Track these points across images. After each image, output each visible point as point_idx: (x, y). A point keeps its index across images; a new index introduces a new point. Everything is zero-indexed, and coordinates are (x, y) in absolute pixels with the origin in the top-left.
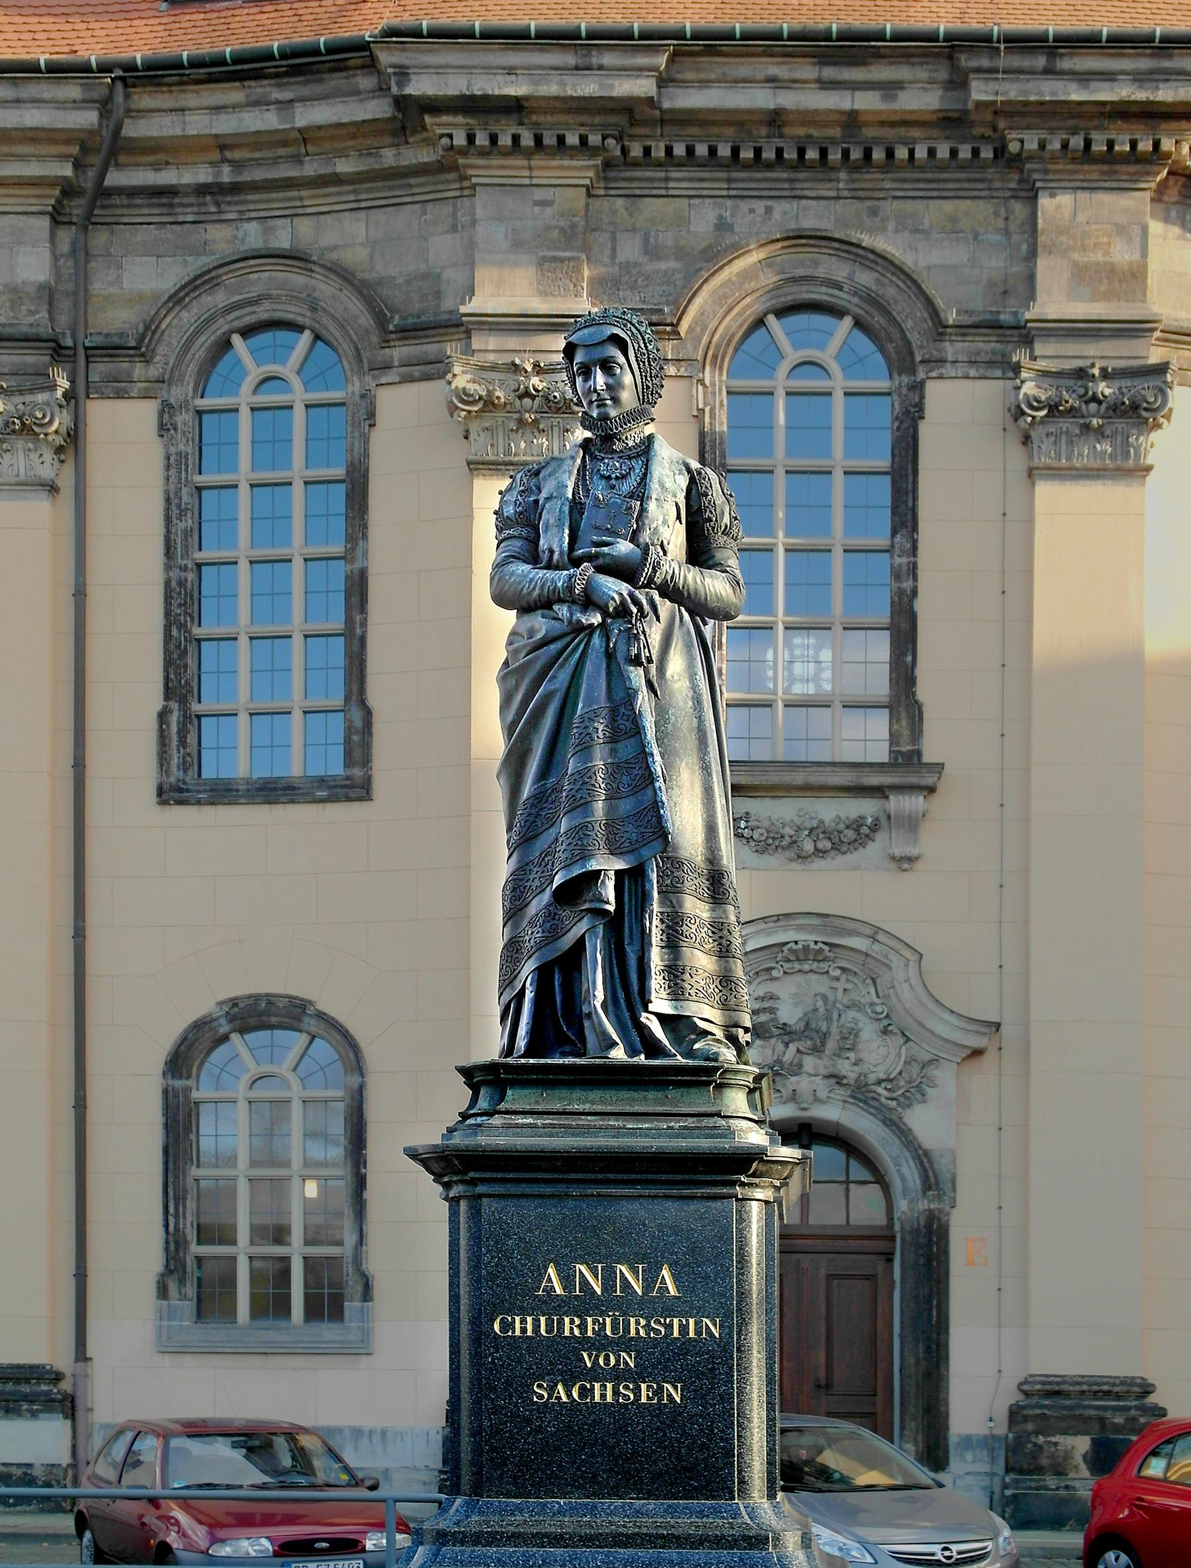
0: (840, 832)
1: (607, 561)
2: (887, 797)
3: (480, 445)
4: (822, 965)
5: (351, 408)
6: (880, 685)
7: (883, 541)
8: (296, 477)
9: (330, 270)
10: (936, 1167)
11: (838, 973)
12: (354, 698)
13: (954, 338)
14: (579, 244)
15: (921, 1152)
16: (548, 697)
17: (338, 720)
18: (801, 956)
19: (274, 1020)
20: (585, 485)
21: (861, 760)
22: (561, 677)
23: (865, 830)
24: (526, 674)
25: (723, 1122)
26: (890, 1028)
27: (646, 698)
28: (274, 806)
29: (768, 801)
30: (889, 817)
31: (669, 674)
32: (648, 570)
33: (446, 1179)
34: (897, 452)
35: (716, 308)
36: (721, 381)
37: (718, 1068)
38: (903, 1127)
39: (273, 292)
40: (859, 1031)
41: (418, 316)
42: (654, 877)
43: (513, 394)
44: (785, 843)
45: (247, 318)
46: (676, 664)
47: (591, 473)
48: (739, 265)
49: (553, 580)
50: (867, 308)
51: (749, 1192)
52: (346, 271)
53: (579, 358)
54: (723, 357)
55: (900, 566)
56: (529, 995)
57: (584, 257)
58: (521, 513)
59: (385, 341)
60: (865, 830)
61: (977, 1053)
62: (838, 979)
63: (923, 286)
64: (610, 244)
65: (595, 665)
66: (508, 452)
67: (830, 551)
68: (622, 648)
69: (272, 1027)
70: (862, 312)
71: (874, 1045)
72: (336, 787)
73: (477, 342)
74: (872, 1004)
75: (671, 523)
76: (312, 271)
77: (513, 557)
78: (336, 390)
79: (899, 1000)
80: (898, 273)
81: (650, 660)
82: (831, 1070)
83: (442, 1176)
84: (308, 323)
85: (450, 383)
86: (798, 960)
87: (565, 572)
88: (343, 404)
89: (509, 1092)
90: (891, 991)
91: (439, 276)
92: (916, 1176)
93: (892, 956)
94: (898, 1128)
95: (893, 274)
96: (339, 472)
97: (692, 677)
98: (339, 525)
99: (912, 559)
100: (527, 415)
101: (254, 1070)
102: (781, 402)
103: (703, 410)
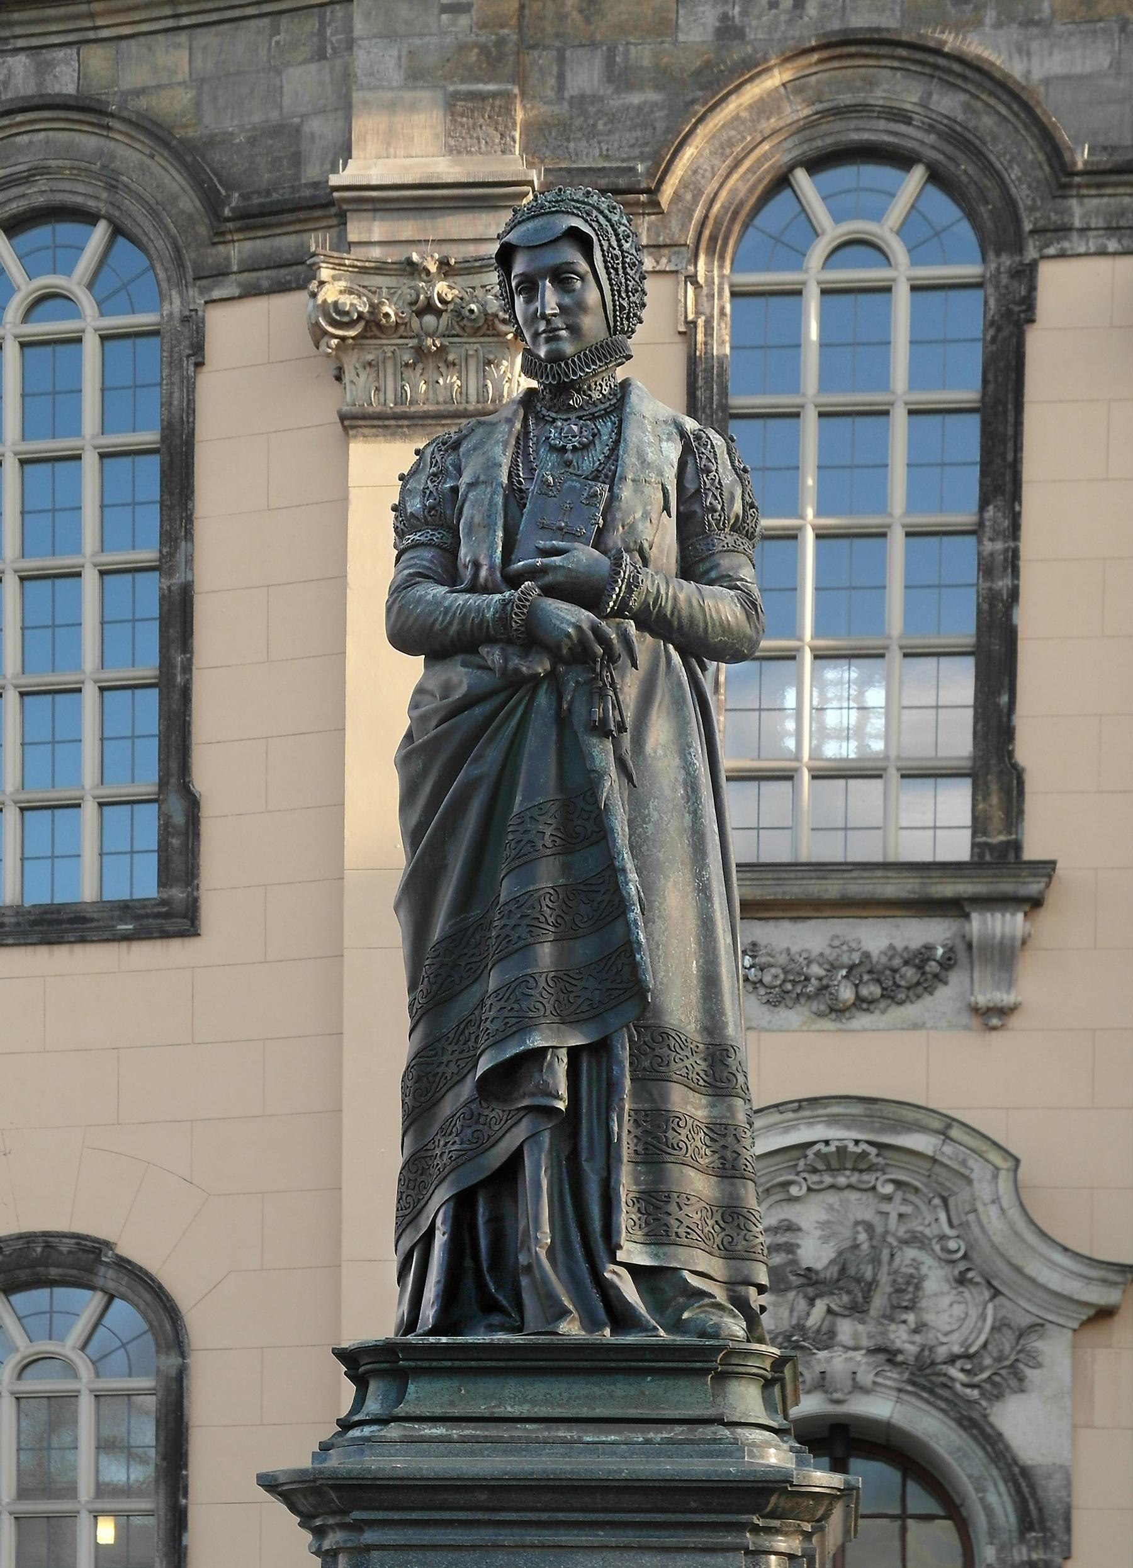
0: (895, 971)
1: (560, 577)
2: (967, 916)
3: (360, 389)
4: (865, 1177)
6: (958, 740)
7: (966, 517)
8: (88, 447)
10: (1040, 1494)
11: (889, 1189)
13: (1084, 191)
15: (1016, 1470)
16: (471, 787)
18: (834, 1163)
19: (54, 1272)
20: (527, 462)
21: (928, 858)
22: (491, 756)
23: (932, 967)
24: (444, 764)
25: (726, 1432)
26: (970, 1275)
27: (616, 786)
28: (56, 948)
29: (786, 925)
30: (970, 946)
32: (620, 588)
33: (318, 1522)
34: (990, 377)
35: (716, 162)
36: (722, 276)
37: (719, 1349)
38: (989, 1430)
39: (53, 163)
40: (922, 1278)
41: (268, 193)
42: (624, 1054)
43: (407, 309)
44: (810, 989)
45: (14, 205)
46: (660, 733)
48: (753, 92)
49: (479, 610)
50: (949, 149)
51: (765, 1541)
52: (159, 126)
53: (519, 267)
54: (726, 239)
55: (992, 554)
56: (440, 1239)
57: (516, 91)
58: (432, 508)
59: (218, 234)
60: (932, 967)
61: (1104, 1314)
62: (889, 1198)
63: (1039, 111)
64: (555, 69)
65: (539, 739)
66: (400, 399)
67: (884, 535)
68: (580, 709)
69: (52, 1283)
70: (940, 157)
71: (945, 1301)
72: (147, 916)
73: (355, 231)
74: (943, 1238)
75: (654, 516)
76: (109, 128)
77: (419, 575)
78: (144, 310)
79: (983, 1230)
80: (999, 91)
81: (621, 727)
82: (880, 1341)
83: (314, 1517)
84: (103, 208)
85: (314, 295)
86: (830, 1169)
87: (498, 597)
88: (156, 333)
89: (411, 1388)
90: (971, 1217)
91: (298, 130)
92: (1010, 1509)
93: (974, 1164)
94: (982, 1431)
95: (991, 94)
96: (150, 437)
97: (684, 751)
98: (151, 519)
99: (1012, 544)
100: (430, 341)
101: (24, 1348)
102: (813, 303)
103: (694, 323)
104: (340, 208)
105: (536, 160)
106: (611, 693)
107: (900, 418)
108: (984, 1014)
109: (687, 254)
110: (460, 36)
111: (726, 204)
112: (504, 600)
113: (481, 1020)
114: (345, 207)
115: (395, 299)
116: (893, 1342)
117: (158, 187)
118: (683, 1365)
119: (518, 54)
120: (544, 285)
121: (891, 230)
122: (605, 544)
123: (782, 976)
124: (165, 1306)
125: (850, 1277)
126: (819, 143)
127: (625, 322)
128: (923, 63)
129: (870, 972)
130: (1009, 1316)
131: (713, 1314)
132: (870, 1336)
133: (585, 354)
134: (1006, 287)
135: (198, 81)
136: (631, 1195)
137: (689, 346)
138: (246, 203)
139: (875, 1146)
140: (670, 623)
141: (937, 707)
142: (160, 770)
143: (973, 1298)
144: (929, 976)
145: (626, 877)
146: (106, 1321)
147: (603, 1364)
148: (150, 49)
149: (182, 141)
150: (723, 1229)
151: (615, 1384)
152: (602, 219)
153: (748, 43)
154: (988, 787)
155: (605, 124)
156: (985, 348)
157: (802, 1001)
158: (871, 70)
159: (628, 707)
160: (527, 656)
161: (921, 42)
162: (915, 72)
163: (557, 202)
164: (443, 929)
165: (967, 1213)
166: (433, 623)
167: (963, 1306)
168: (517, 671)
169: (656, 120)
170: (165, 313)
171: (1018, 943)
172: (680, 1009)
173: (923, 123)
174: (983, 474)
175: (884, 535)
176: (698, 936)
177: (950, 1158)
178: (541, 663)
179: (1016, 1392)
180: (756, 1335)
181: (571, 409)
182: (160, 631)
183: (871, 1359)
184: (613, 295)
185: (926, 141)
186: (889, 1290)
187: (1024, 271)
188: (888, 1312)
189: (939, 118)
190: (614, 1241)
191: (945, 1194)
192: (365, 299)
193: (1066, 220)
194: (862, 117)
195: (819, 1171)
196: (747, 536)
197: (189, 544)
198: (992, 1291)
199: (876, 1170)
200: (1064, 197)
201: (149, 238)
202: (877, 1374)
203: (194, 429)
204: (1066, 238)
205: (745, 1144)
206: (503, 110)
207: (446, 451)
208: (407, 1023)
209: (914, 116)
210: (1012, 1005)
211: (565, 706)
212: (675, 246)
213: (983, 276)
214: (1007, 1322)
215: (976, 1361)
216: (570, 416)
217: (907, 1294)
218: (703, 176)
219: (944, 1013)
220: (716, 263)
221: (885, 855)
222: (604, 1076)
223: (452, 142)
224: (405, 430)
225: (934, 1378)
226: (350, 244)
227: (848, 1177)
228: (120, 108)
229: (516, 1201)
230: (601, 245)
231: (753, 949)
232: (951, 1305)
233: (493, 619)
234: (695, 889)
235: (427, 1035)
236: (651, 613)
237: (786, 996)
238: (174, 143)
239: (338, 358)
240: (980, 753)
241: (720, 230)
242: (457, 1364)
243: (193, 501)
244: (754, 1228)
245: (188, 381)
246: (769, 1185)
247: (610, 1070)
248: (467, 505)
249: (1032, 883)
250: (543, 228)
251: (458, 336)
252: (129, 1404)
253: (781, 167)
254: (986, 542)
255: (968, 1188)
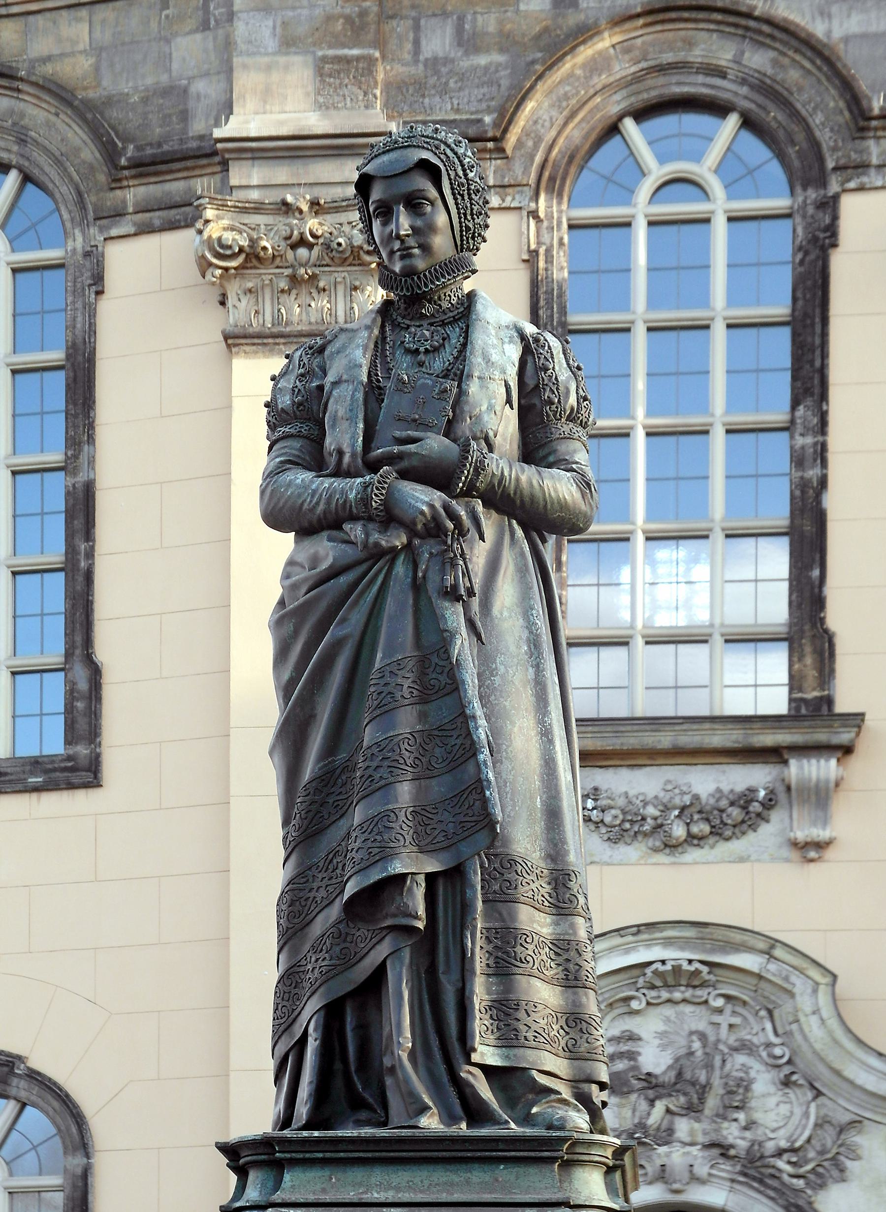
0: (722, 811)
1: (415, 462)
2: (785, 762)
3: (241, 311)
4: (699, 992)
5: (71, 271)
6: (775, 608)
9: (42, 87)
11: (720, 1002)
12: (78, 652)
14: (370, 36)
16: (337, 646)
17: (56, 684)
18: (670, 980)
20: (385, 363)
21: (750, 712)
22: (354, 619)
24: (310, 625)
26: (794, 1078)
27: (466, 644)
29: (625, 773)
30: (789, 789)
31: (496, 610)
32: (468, 471)
34: (799, 294)
35: (554, 113)
36: (560, 212)
37: (564, 1140)
40: (751, 1081)
41: (159, 145)
42: (477, 879)
43: (283, 244)
44: (647, 828)
46: (506, 593)
47: (392, 347)
48: (585, 53)
49: (343, 492)
50: (760, 99)
53: (376, 194)
55: (803, 448)
57: (377, 54)
58: (300, 404)
60: (755, 807)
63: (839, 65)
64: (411, 36)
70: (752, 106)
71: (772, 1101)
72: (55, 770)
73: (238, 175)
74: (769, 1045)
75: (498, 408)
76: (19, 90)
80: (804, 49)
81: (471, 593)
82: (714, 1137)
85: (200, 232)
86: (666, 985)
88: (61, 266)
89: (287, 1177)
90: (794, 1027)
91: (185, 91)
95: (796, 51)
96: (56, 355)
97: (527, 613)
99: (820, 438)
100: (302, 271)
104: (223, 157)
105: (396, 114)
106: (461, 563)
107: (719, 331)
108: (803, 848)
109: (528, 192)
110: (327, 8)
111: (564, 149)
112: (365, 483)
113: (348, 851)
114: (227, 156)
115: (272, 234)
116: (726, 1138)
117: (62, 140)
118: (532, 1154)
119: (379, 23)
120: (398, 210)
121: (710, 169)
122: (455, 433)
123: (621, 817)
124: (72, 1112)
125: (685, 1080)
126: (645, 96)
127: (471, 241)
128: (736, 26)
129: (700, 812)
130: (830, 1114)
131: (559, 1108)
132: (705, 1133)
133: (435, 269)
134: (812, 217)
135: (97, 50)
136: (483, 1004)
137: (532, 272)
138: (140, 154)
139: (706, 966)
140: (513, 501)
141: (756, 581)
142: (66, 643)
143: (798, 1099)
144: (753, 815)
145: (476, 723)
146: (18, 1126)
147: (460, 1154)
148: (54, 23)
149: (82, 101)
150: (567, 1033)
151: (470, 1172)
152: (448, 151)
153: (582, 11)
154: (803, 650)
155: (456, 82)
156: (794, 269)
157: (640, 838)
158: (690, 33)
159: (476, 575)
160: (386, 531)
161: (734, 7)
162: (729, 33)
163: (409, 137)
164: (313, 771)
165: (790, 1024)
166: (302, 504)
167: (788, 1106)
168: (377, 544)
169: (501, 78)
170: (69, 249)
171: (832, 785)
172: (525, 842)
173: (737, 77)
174: (794, 378)
175: (707, 432)
176: (542, 774)
177: (774, 975)
178: (399, 537)
179: (837, 1182)
180: (599, 1127)
181: (423, 317)
182: (66, 522)
183: (707, 1153)
184: (460, 218)
185: (740, 92)
186: (722, 1091)
187: (827, 203)
188: (721, 1111)
189: (751, 73)
190: (469, 1044)
191: (771, 1006)
192: (245, 235)
193: (865, 158)
194: (683, 73)
195: (657, 987)
196: (581, 424)
197: (91, 447)
198: (815, 1092)
199: (709, 986)
200: (863, 138)
201: (55, 184)
202: (712, 1167)
203: (95, 349)
204: (863, 174)
205: (586, 958)
206: (366, 72)
207: (313, 354)
208: (282, 854)
209: (729, 71)
210: (827, 839)
211: (420, 575)
212: (519, 185)
213: (792, 208)
214: (828, 1119)
215: (801, 1154)
216: (422, 323)
217: (737, 1096)
218: (543, 126)
219: (767, 847)
220: (555, 201)
221: (711, 709)
222: (459, 898)
223: (321, 100)
224: (282, 347)
225: (763, 1170)
226: (232, 188)
227: (683, 992)
228: (29, 73)
229: (379, 1009)
230: (449, 175)
231: (594, 793)
232: (778, 1105)
233: (356, 500)
234: (538, 733)
235: (299, 864)
236: (496, 493)
237: (625, 834)
238: (76, 103)
239: (222, 286)
240: (796, 620)
241: (558, 171)
242: (328, 1155)
243: (94, 410)
244: (595, 1032)
245: (90, 307)
246: (611, 1000)
247: (463, 893)
248: (331, 401)
249: (844, 732)
250: (397, 160)
251: (327, 265)
252: (40, 1200)
253: (610, 117)
254: (797, 437)
255: (791, 1001)
